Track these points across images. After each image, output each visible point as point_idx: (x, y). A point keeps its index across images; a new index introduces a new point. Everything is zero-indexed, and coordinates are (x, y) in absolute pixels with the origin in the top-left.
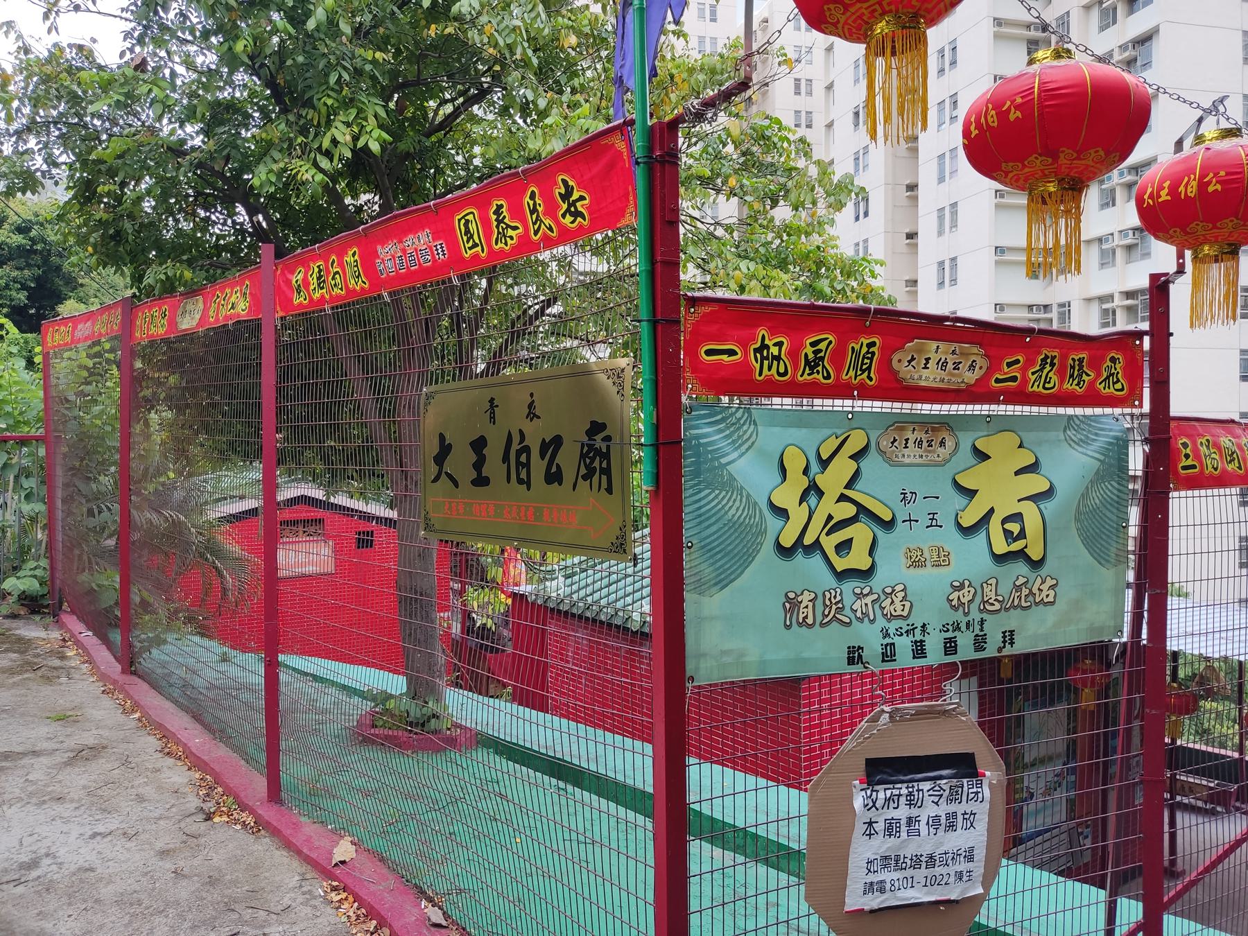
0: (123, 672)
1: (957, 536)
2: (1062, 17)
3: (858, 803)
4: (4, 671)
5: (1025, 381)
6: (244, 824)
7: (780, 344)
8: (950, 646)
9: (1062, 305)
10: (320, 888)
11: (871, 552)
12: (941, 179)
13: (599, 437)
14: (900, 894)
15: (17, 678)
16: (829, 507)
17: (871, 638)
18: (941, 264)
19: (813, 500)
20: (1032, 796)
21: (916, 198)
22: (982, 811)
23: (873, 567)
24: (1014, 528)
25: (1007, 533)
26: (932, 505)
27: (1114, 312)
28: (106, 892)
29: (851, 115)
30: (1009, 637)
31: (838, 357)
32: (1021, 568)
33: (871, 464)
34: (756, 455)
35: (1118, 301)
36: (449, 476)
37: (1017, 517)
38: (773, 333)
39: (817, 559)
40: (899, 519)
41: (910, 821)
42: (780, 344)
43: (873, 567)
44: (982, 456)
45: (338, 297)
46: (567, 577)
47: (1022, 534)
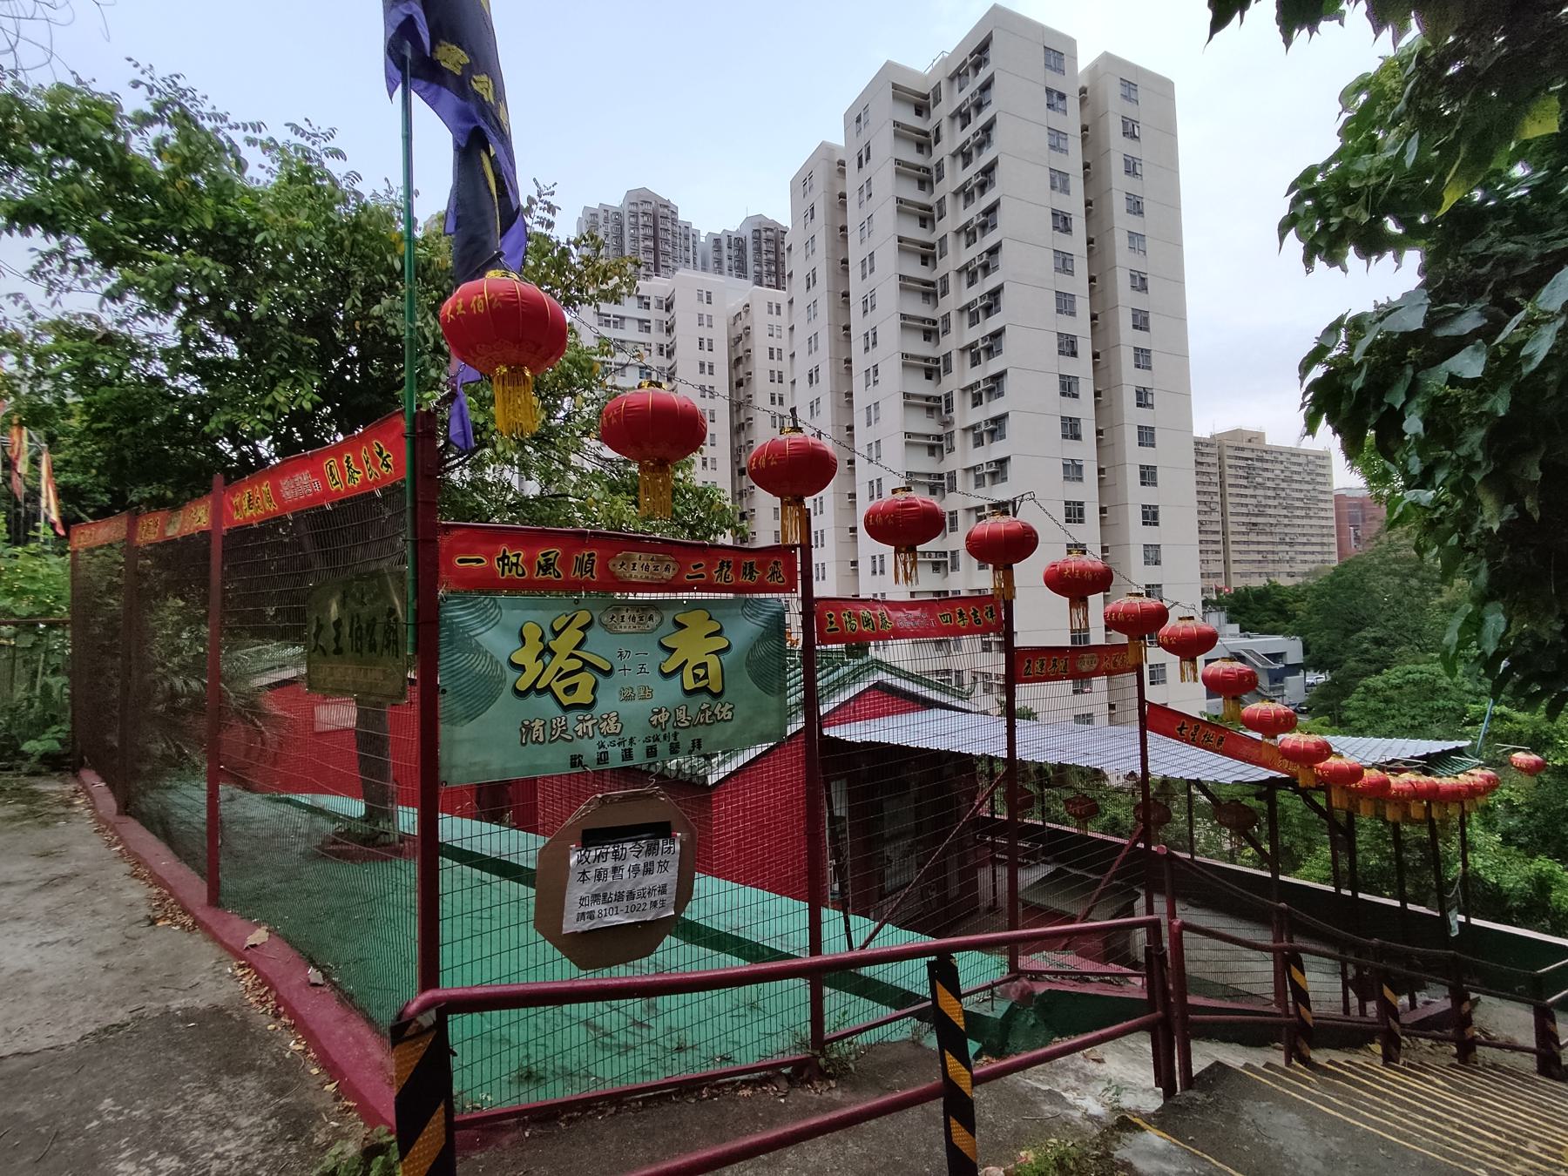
0: (119, 813)
3: (573, 860)
4: (3, 819)
6: (183, 926)
7: (518, 556)
11: (594, 691)
12: (869, 424)
14: (608, 919)
15: (17, 824)
16: (561, 662)
17: (590, 750)
19: (547, 658)
23: (594, 701)
24: (701, 672)
25: (696, 676)
28: (37, 987)
31: (565, 563)
32: (705, 699)
37: (704, 665)
38: (512, 548)
40: (616, 668)
41: (615, 869)
42: (518, 556)
43: (594, 701)
44: (680, 626)
47: (706, 676)
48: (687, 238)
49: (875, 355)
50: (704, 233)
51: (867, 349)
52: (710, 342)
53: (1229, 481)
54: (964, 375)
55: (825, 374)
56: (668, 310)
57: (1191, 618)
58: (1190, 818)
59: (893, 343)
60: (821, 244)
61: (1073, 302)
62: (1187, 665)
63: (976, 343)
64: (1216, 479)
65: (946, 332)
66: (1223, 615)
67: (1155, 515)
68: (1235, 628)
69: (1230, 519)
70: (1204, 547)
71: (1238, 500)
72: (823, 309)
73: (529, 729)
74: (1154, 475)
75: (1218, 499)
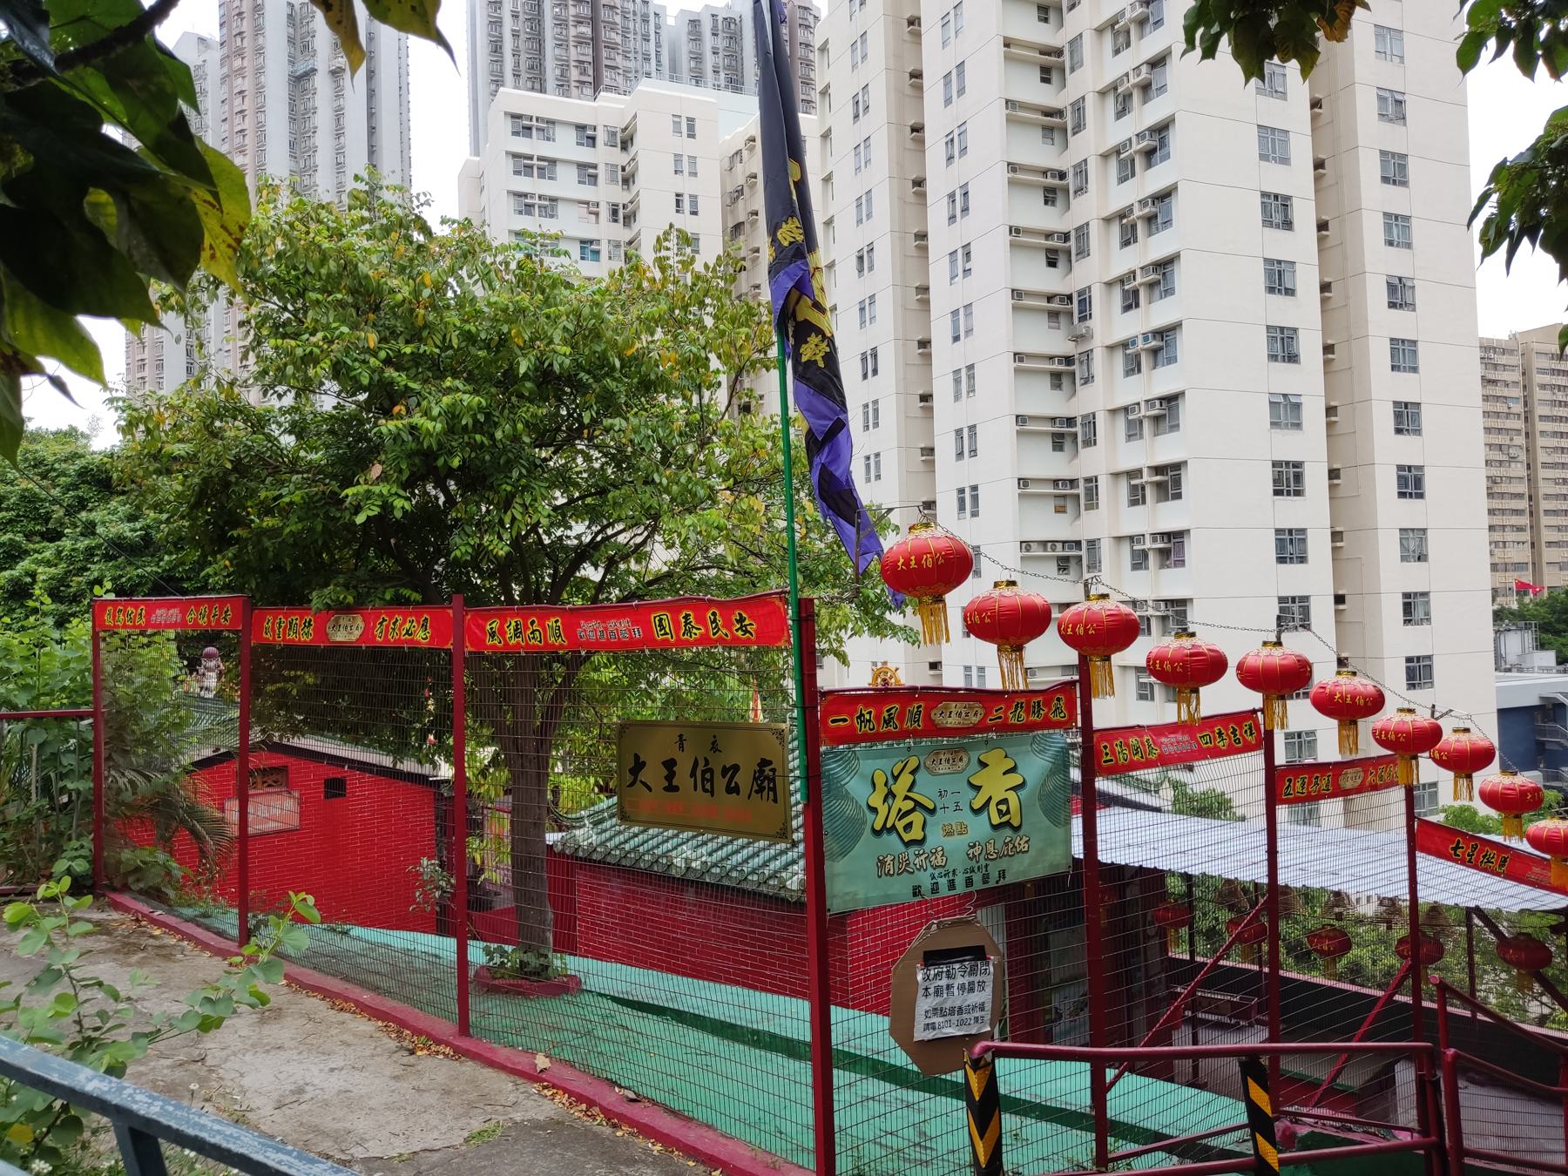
1: (971, 815)
2: (1079, 164)
3: (920, 977)
5: (1007, 718)
8: (969, 882)
9: (1088, 480)
10: (534, 1088)
13: (767, 769)
17: (924, 879)
18: (959, 432)
20: (1060, 1016)
21: (930, 355)
22: (989, 979)
24: (1003, 807)
25: (1000, 811)
26: (956, 797)
27: (1143, 488)
29: (854, 261)
30: (1002, 874)
31: (901, 717)
32: (1008, 832)
33: (922, 776)
34: (861, 779)
35: (1146, 477)
36: (644, 784)
37: (1005, 801)
38: (866, 707)
39: (894, 835)
41: (948, 987)
44: (984, 765)
45: (534, 646)
46: (596, 824)
47: (1008, 812)
48: (645, 20)
49: (966, 229)
51: (952, 218)
52: (694, 199)
53: (1541, 410)
54: (1107, 260)
55: (883, 257)
56: (624, 147)
57: (1467, 730)
58: (1471, 964)
59: (997, 208)
60: (878, 46)
61: (1286, 142)
62: (1463, 782)
63: (1130, 209)
64: (1518, 408)
65: (1080, 190)
66: (1529, 637)
67: (1418, 482)
68: (1549, 657)
69: (1543, 473)
70: (1497, 520)
71: (1554, 442)
72: (881, 151)
73: (882, 863)
74: (1416, 417)
75: (1520, 440)
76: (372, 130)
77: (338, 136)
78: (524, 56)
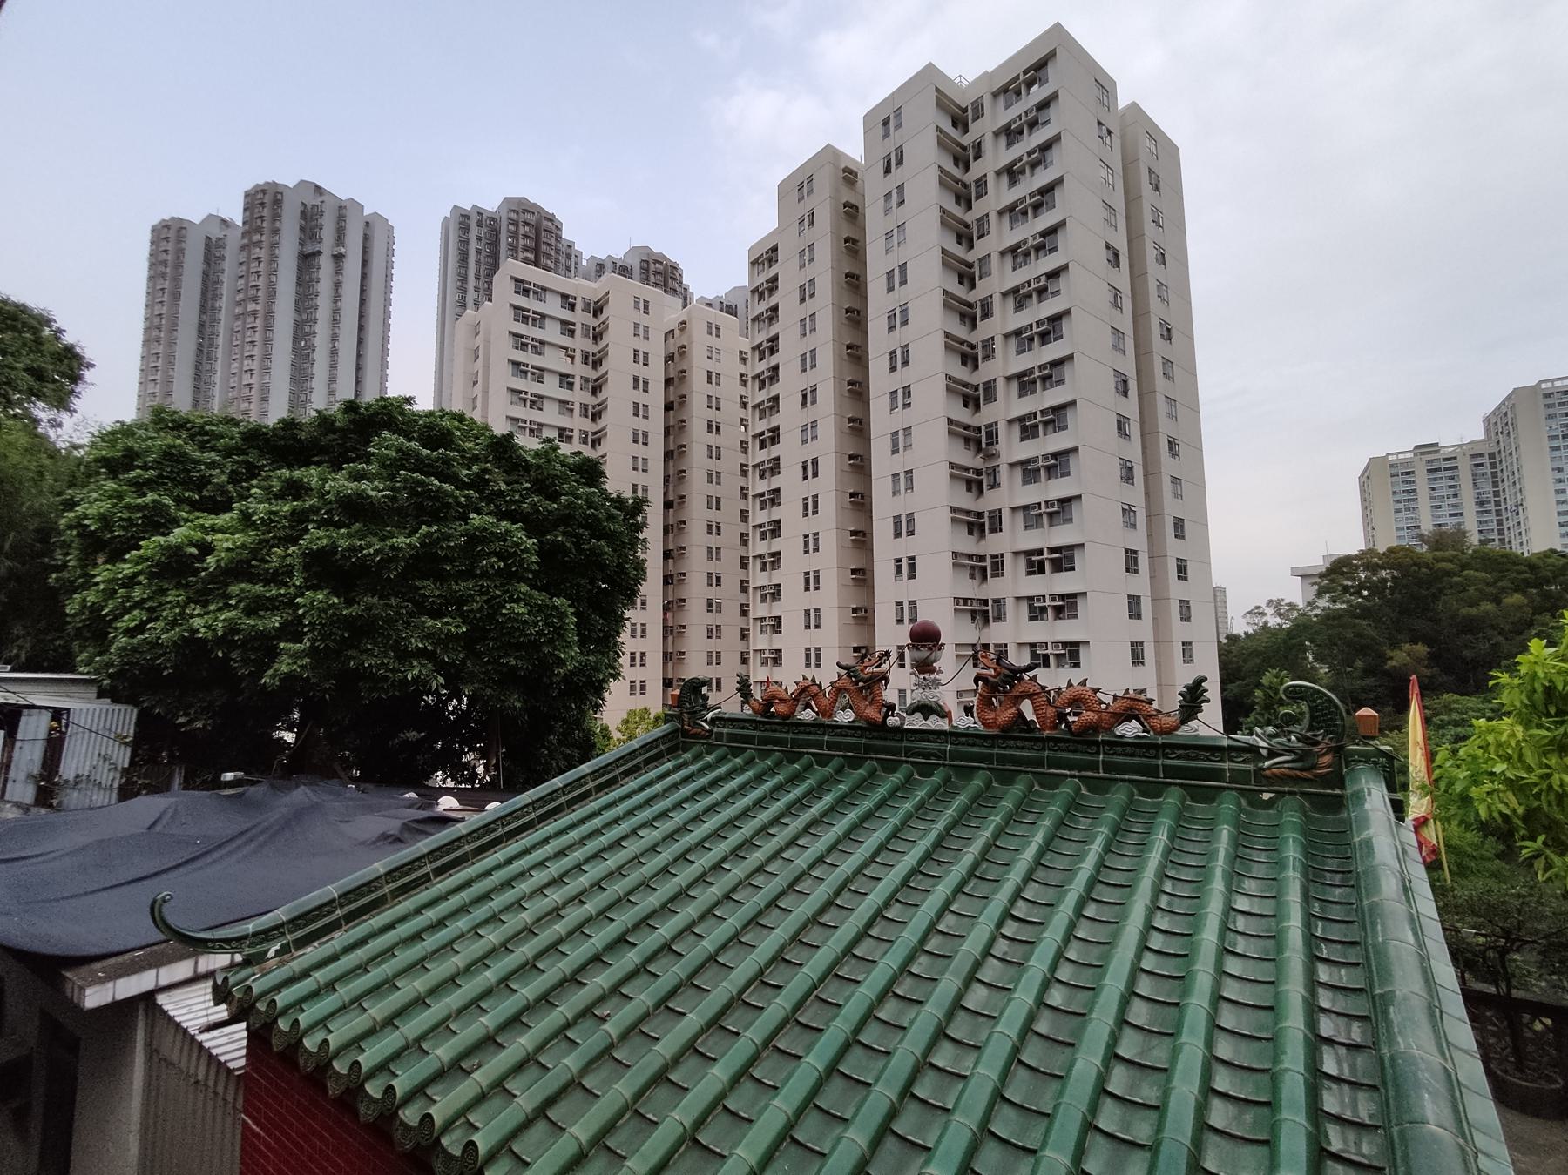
50: (586, 256)
52: (646, 355)
76: (363, 302)
77: (336, 301)
78: (483, 267)
